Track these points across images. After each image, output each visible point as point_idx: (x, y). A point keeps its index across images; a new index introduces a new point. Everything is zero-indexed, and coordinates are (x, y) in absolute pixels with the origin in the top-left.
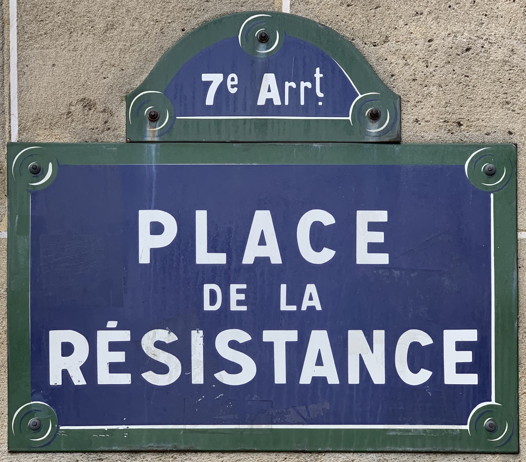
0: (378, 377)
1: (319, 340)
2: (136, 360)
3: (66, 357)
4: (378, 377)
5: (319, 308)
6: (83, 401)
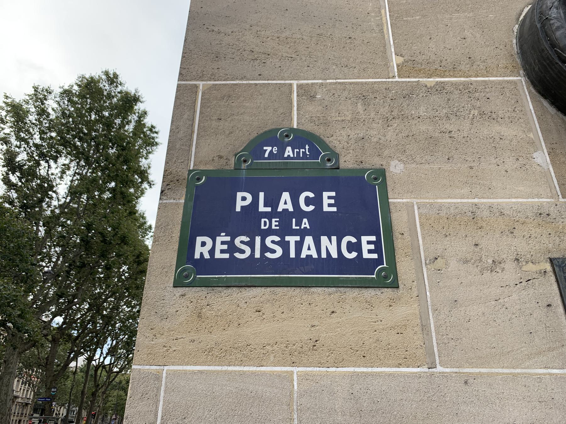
0: (335, 255)
3: (202, 248)
4: (335, 255)
5: (308, 227)
6: (209, 265)
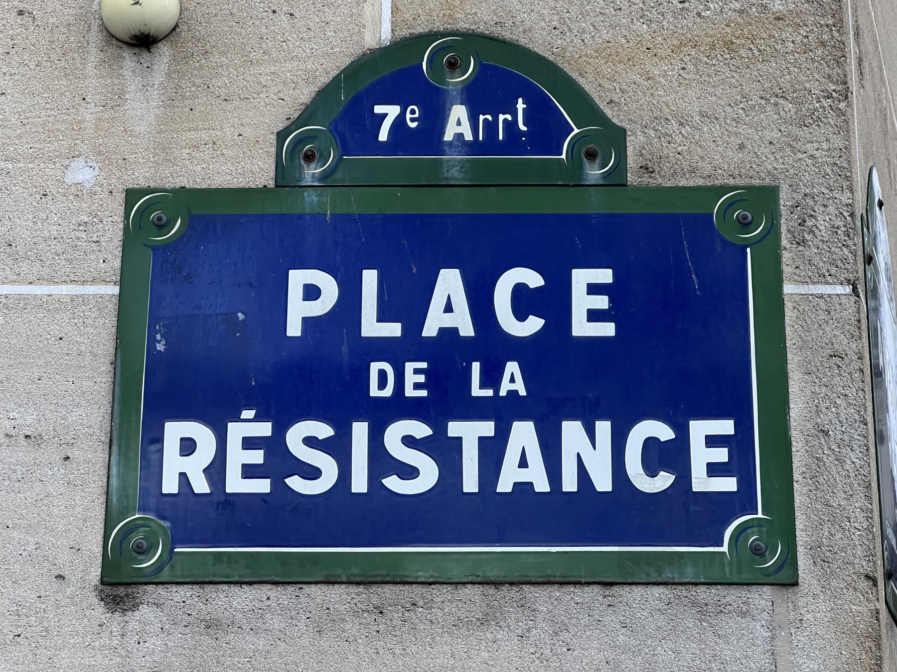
0: (603, 482)
1: (524, 435)
2: (278, 461)
3: (186, 455)
4: (603, 482)
5: (523, 392)
6: (214, 518)
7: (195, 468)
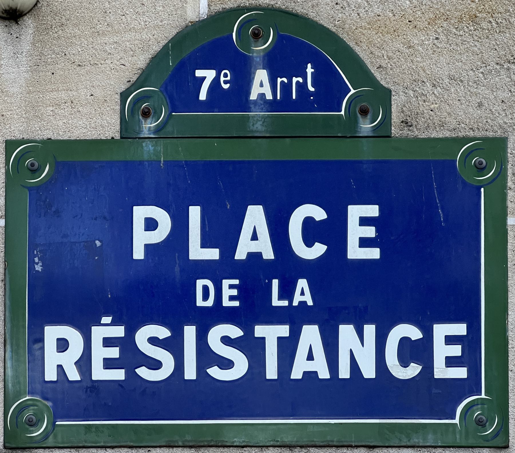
0: (369, 371)
1: (311, 335)
2: (130, 356)
4: (369, 371)
5: (310, 303)
7: (69, 360)
